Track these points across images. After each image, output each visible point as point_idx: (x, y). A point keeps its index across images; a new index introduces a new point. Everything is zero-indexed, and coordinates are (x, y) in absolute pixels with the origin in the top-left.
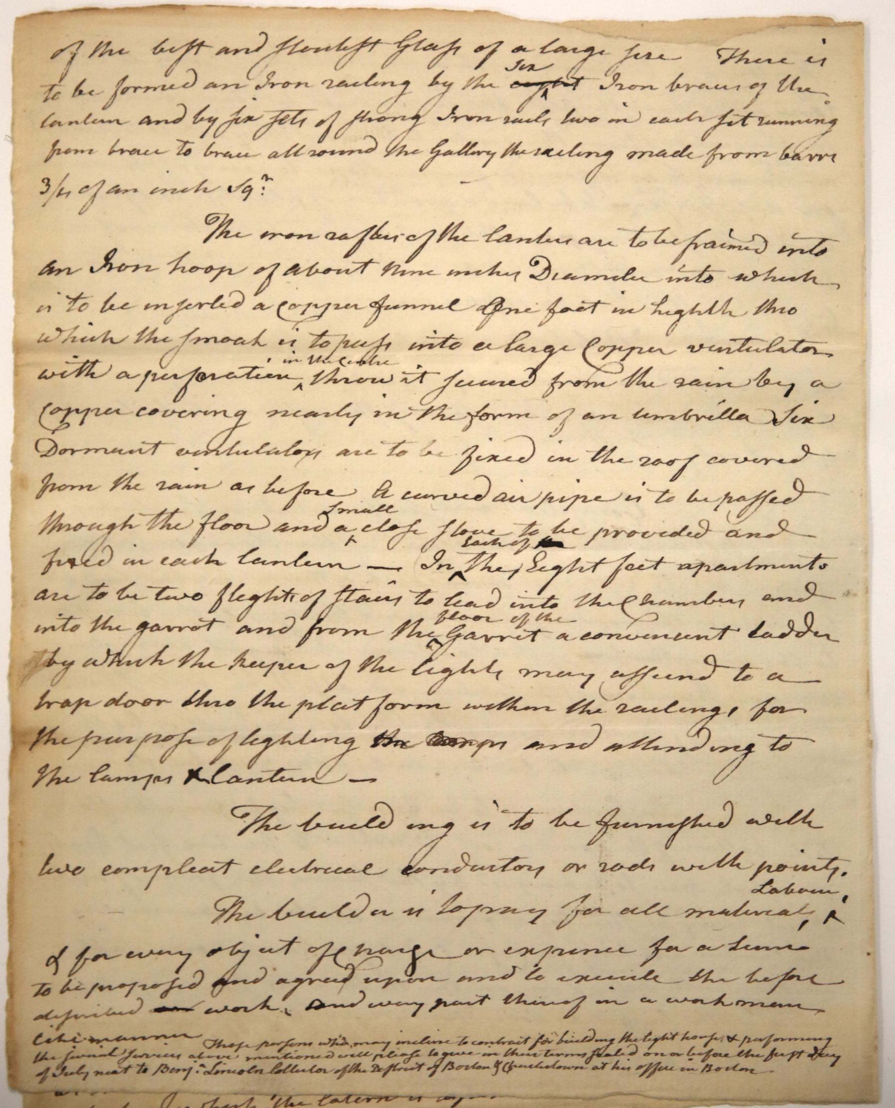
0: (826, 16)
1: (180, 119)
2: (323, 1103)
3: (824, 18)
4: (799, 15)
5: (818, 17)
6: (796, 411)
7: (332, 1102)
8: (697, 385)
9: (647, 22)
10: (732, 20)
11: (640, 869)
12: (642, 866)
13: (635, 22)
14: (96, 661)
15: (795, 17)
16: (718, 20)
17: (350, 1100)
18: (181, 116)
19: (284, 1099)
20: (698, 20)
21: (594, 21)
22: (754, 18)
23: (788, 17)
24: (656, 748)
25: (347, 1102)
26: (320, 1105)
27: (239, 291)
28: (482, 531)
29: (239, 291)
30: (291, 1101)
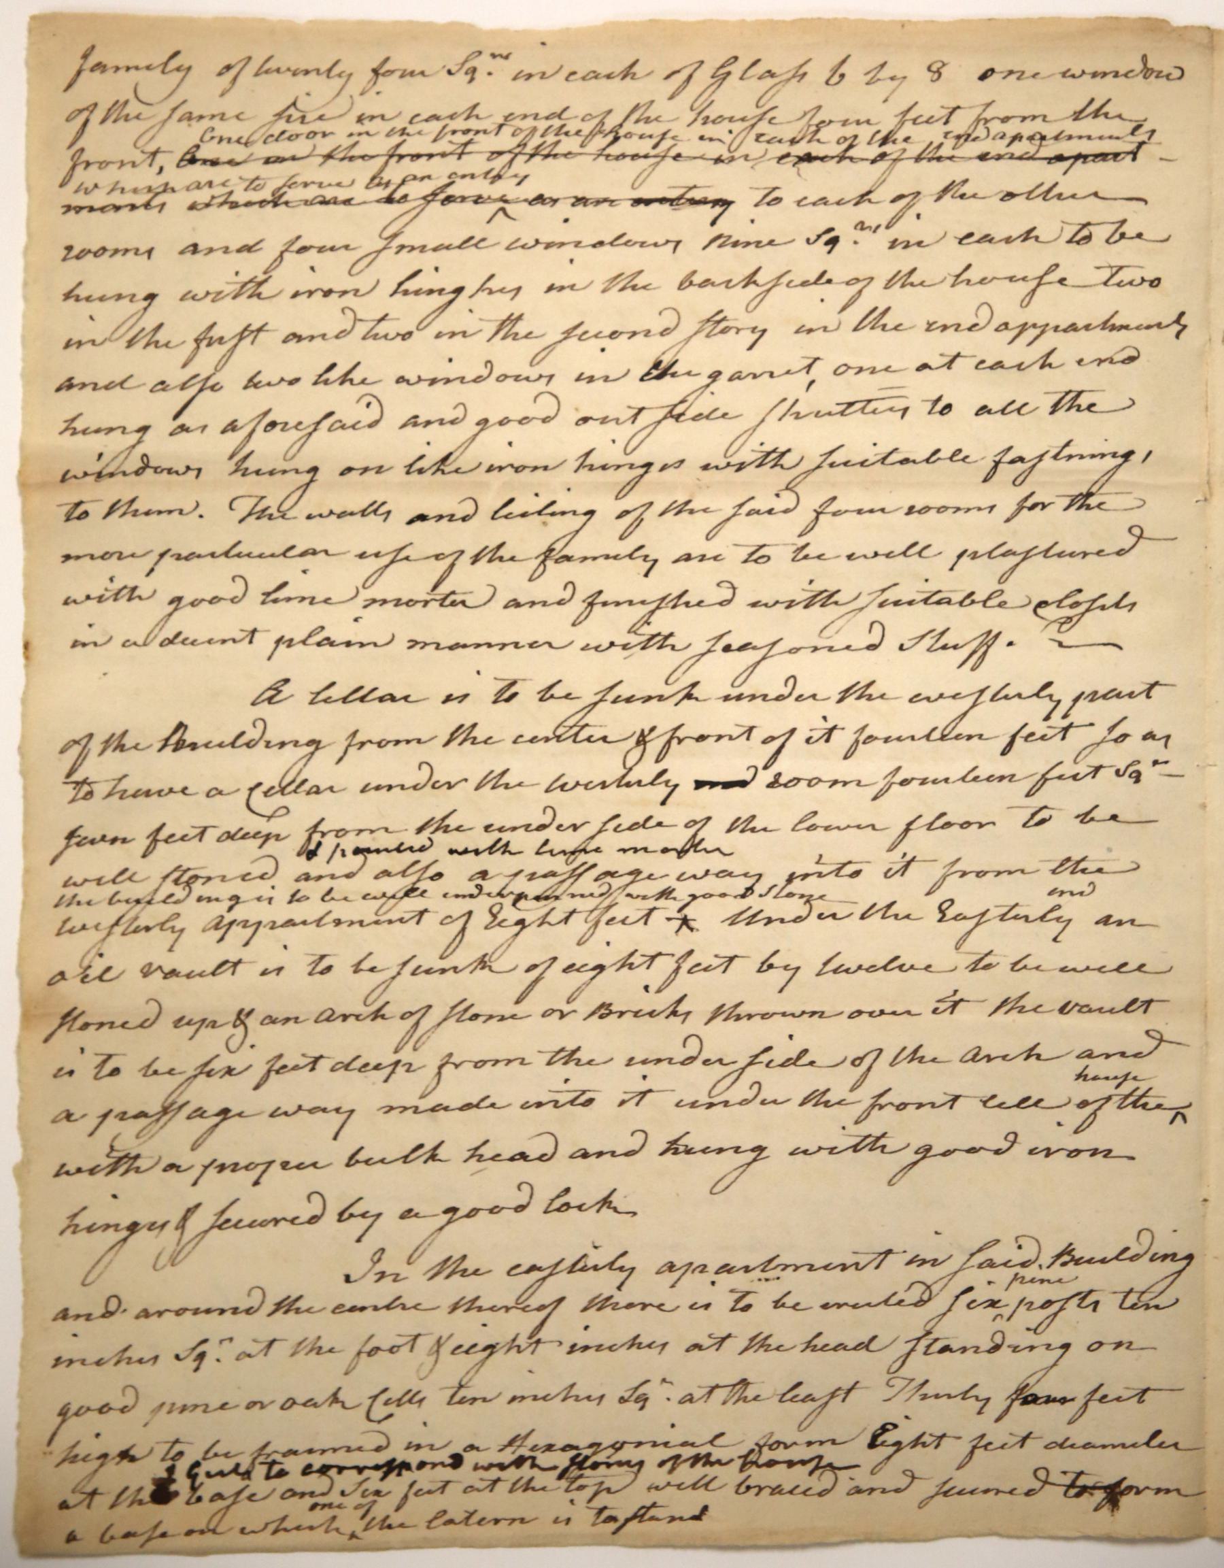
0: (1161, 17)
1: (377, 422)
2: (433, 1525)
3: (1157, 20)
4: (1122, 15)
5: (1148, 19)
6: (834, 455)
7: (445, 1523)
8: (163, 390)
9: (909, 21)
10: (1029, 21)
11: (641, 830)
12: (644, 826)
13: (893, 22)
14: (134, 874)
15: (1117, 18)
16: (1009, 20)
17: (471, 1521)
18: (378, 417)
19: (378, 1519)
20: (980, 20)
21: (835, 19)
22: (1059, 18)
23: (1107, 18)
24: (421, 471)
25: (466, 1524)
26: (428, 1527)
27: (1037, 1241)
28: (912, 967)
29: (1037, 1241)
30: (388, 1522)
